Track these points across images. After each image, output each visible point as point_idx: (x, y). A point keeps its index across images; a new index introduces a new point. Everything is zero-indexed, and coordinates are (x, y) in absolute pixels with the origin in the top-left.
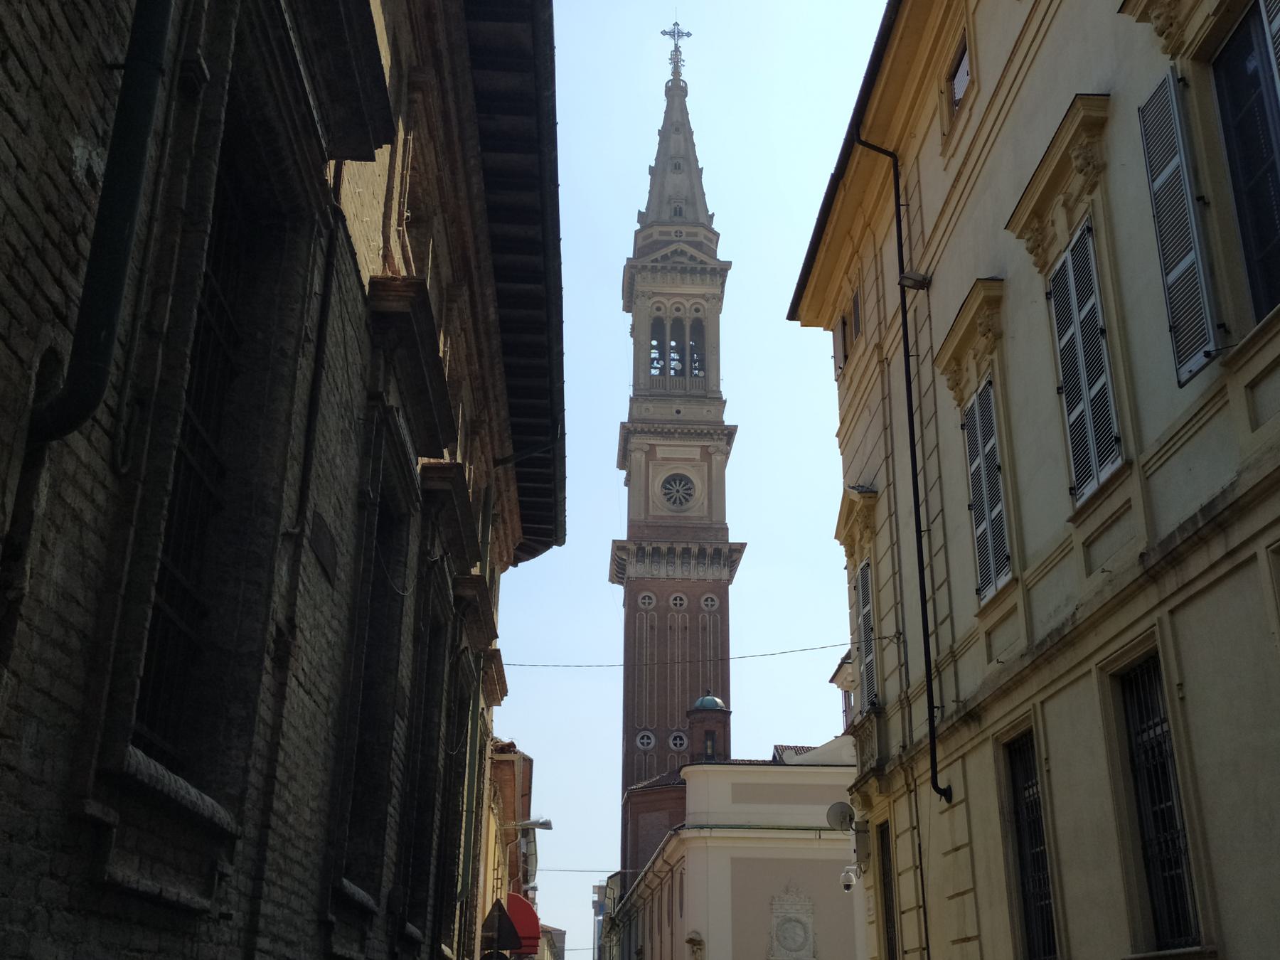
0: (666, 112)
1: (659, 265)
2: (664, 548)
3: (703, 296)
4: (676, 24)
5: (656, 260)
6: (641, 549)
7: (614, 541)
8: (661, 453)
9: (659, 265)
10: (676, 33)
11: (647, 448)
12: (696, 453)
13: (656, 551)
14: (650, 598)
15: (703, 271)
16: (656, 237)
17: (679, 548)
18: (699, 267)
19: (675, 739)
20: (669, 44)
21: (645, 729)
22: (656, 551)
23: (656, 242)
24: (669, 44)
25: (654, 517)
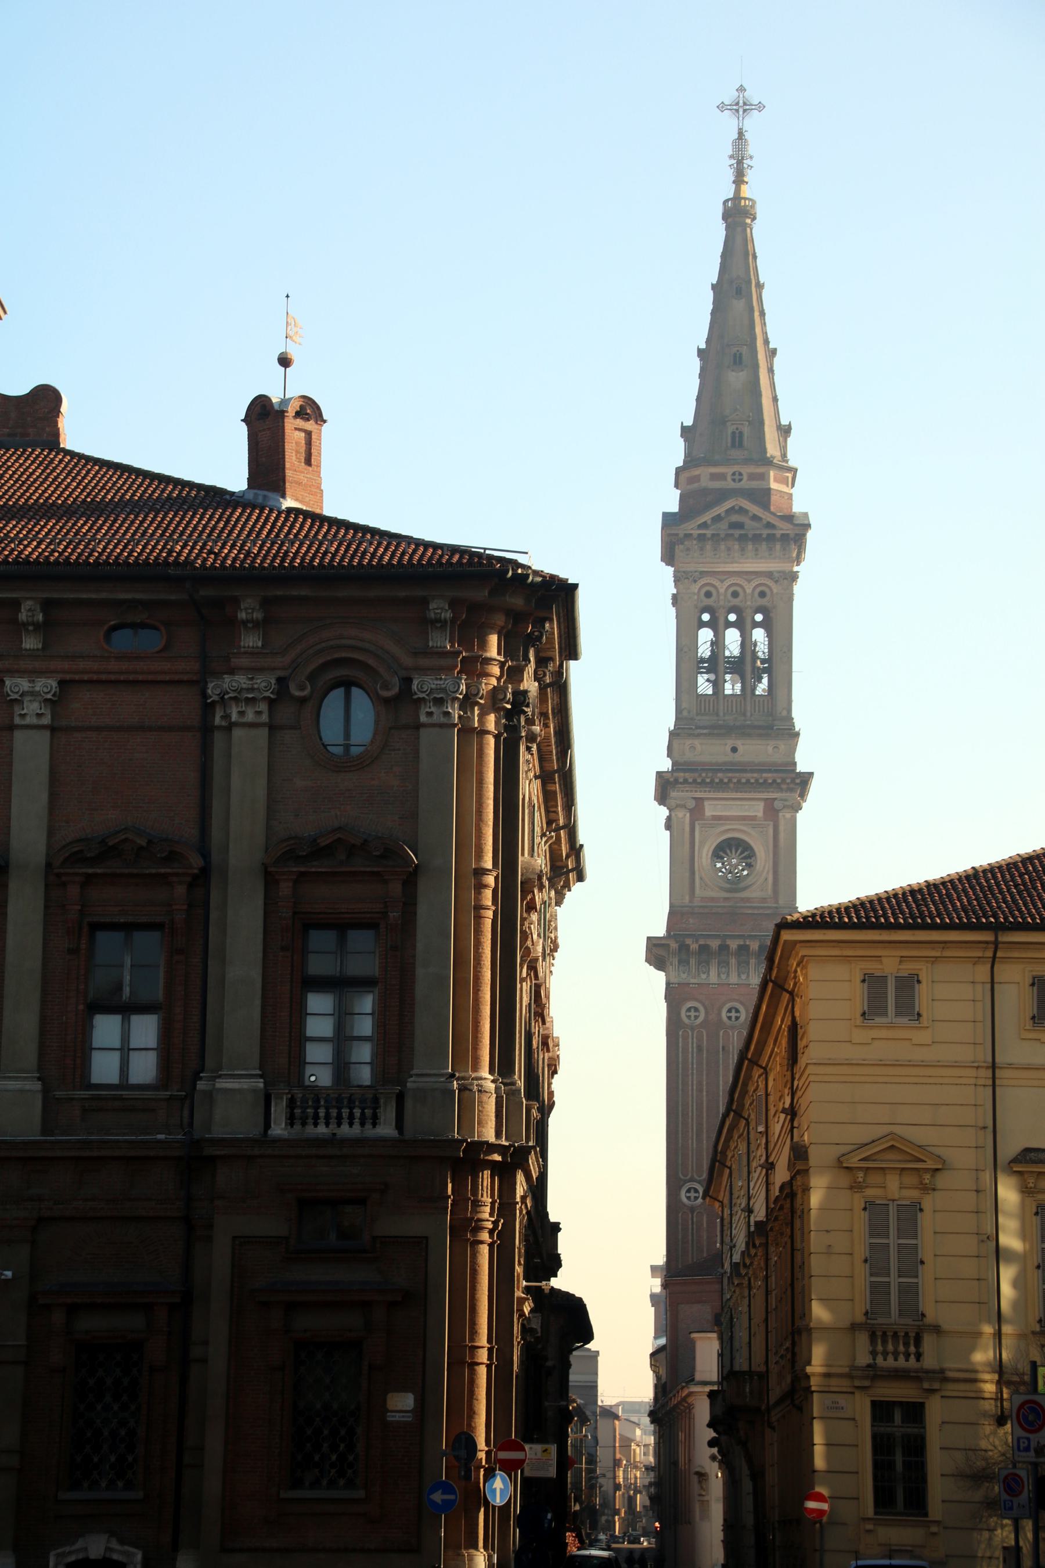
0: (713, 313)
1: (708, 532)
2: (714, 944)
3: (769, 575)
4: (741, 89)
5: (704, 525)
6: (683, 948)
7: (649, 938)
8: (709, 811)
9: (708, 532)
10: (741, 107)
11: (691, 804)
12: (757, 809)
13: (704, 949)
14: (696, 1010)
15: (771, 538)
16: (705, 483)
17: (733, 945)
18: (765, 532)
19: (689, 1191)
20: (729, 125)
21: (692, 1180)
22: (704, 949)
23: (705, 492)
24: (729, 125)
25: (703, 899)
